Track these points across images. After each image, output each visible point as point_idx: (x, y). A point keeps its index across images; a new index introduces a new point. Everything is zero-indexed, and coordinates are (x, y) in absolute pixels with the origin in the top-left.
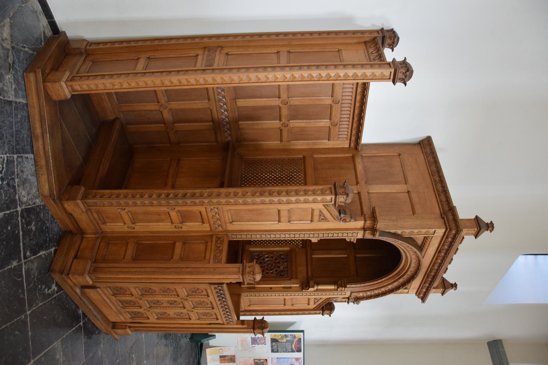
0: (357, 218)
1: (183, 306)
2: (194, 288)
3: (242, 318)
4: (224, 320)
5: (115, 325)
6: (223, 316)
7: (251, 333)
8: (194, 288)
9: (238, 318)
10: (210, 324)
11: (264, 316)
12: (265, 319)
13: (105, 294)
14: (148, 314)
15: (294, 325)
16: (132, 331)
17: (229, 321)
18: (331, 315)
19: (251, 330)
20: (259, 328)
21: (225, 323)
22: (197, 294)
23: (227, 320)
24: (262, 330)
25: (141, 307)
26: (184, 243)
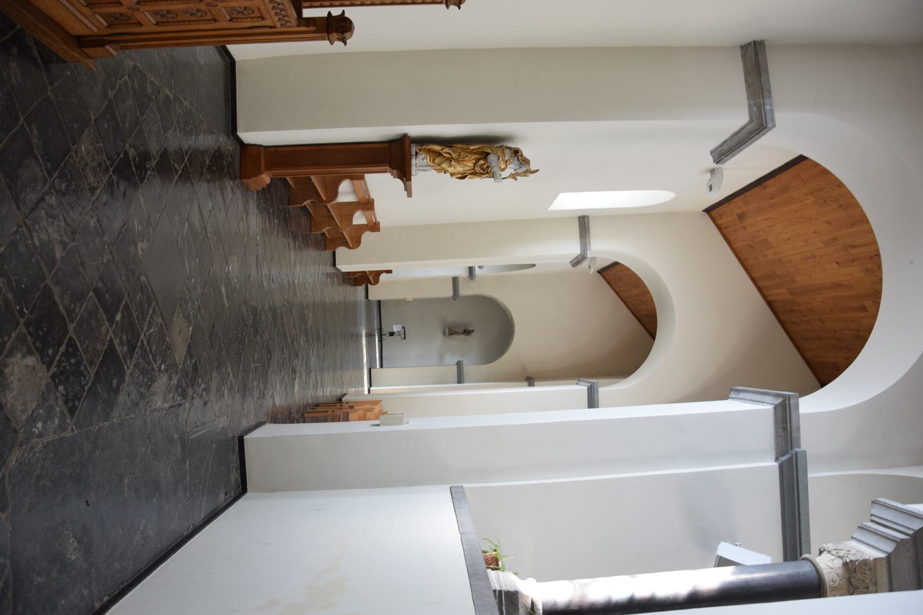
0: (536, 383)
1: (212, 18)
2: (240, 7)
3: (307, 13)
4: (276, 19)
5: (83, 42)
6: (273, 13)
7: (324, 39)
8: (240, 7)
9: (299, 14)
10: (251, 28)
11: (345, 9)
12: (346, 15)
13: (82, 14)
14: (139, 16)
15: (533, 600)
16: (116, 50)
17: (284, 20)
18: (461, 6)
19: (323, 34)
20: (337, 31)
21: (278, 24)
22: (244, 16)
23: (280, 19)
24: (343, 34)
25: (141, 25)
26: (493, 563)
